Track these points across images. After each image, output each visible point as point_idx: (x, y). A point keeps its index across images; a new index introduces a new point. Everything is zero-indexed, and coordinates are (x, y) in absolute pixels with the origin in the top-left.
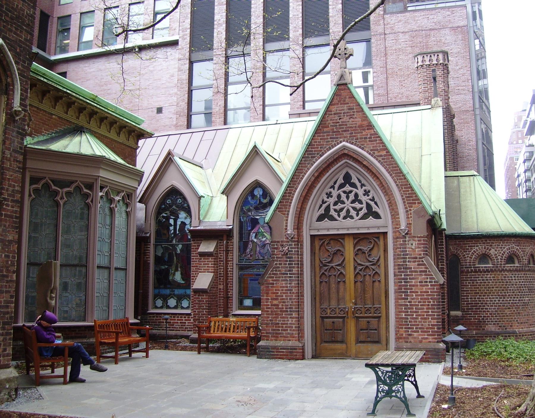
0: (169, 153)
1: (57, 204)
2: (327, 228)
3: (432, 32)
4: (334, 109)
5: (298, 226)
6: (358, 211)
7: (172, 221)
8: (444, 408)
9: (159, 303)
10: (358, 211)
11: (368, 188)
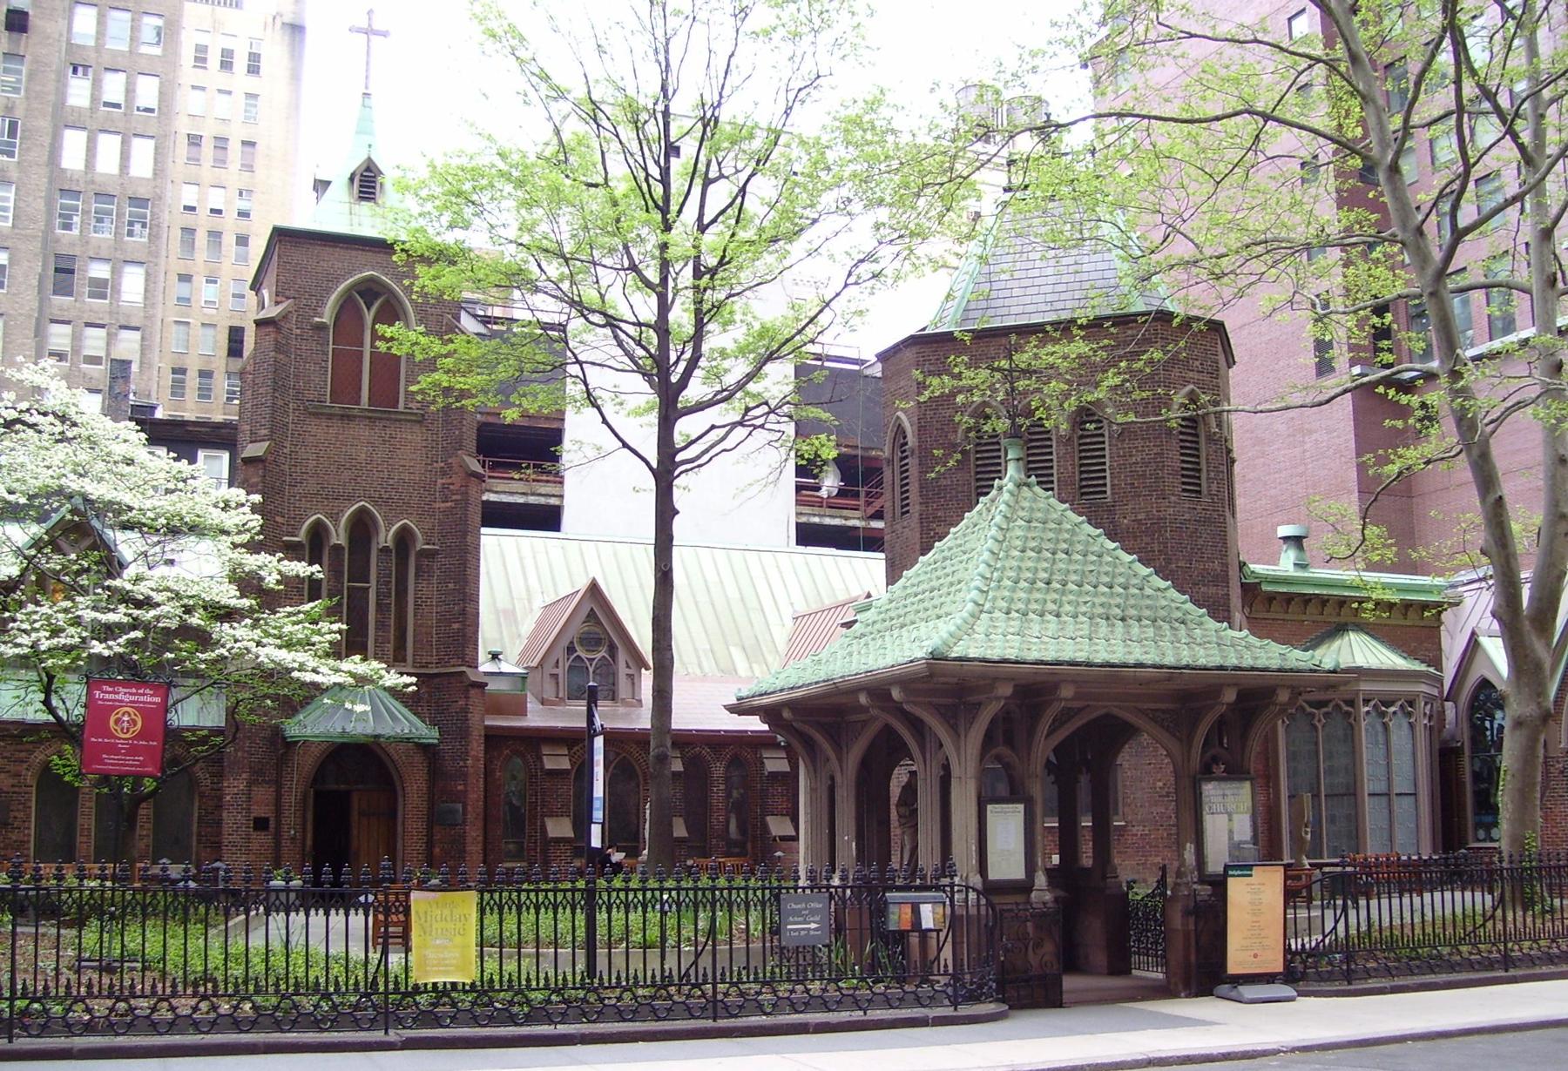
0: (1473, 633)
1: (1316, 728)
7: (1487, 724)
8: (670, 825)
9: (1481, 834)
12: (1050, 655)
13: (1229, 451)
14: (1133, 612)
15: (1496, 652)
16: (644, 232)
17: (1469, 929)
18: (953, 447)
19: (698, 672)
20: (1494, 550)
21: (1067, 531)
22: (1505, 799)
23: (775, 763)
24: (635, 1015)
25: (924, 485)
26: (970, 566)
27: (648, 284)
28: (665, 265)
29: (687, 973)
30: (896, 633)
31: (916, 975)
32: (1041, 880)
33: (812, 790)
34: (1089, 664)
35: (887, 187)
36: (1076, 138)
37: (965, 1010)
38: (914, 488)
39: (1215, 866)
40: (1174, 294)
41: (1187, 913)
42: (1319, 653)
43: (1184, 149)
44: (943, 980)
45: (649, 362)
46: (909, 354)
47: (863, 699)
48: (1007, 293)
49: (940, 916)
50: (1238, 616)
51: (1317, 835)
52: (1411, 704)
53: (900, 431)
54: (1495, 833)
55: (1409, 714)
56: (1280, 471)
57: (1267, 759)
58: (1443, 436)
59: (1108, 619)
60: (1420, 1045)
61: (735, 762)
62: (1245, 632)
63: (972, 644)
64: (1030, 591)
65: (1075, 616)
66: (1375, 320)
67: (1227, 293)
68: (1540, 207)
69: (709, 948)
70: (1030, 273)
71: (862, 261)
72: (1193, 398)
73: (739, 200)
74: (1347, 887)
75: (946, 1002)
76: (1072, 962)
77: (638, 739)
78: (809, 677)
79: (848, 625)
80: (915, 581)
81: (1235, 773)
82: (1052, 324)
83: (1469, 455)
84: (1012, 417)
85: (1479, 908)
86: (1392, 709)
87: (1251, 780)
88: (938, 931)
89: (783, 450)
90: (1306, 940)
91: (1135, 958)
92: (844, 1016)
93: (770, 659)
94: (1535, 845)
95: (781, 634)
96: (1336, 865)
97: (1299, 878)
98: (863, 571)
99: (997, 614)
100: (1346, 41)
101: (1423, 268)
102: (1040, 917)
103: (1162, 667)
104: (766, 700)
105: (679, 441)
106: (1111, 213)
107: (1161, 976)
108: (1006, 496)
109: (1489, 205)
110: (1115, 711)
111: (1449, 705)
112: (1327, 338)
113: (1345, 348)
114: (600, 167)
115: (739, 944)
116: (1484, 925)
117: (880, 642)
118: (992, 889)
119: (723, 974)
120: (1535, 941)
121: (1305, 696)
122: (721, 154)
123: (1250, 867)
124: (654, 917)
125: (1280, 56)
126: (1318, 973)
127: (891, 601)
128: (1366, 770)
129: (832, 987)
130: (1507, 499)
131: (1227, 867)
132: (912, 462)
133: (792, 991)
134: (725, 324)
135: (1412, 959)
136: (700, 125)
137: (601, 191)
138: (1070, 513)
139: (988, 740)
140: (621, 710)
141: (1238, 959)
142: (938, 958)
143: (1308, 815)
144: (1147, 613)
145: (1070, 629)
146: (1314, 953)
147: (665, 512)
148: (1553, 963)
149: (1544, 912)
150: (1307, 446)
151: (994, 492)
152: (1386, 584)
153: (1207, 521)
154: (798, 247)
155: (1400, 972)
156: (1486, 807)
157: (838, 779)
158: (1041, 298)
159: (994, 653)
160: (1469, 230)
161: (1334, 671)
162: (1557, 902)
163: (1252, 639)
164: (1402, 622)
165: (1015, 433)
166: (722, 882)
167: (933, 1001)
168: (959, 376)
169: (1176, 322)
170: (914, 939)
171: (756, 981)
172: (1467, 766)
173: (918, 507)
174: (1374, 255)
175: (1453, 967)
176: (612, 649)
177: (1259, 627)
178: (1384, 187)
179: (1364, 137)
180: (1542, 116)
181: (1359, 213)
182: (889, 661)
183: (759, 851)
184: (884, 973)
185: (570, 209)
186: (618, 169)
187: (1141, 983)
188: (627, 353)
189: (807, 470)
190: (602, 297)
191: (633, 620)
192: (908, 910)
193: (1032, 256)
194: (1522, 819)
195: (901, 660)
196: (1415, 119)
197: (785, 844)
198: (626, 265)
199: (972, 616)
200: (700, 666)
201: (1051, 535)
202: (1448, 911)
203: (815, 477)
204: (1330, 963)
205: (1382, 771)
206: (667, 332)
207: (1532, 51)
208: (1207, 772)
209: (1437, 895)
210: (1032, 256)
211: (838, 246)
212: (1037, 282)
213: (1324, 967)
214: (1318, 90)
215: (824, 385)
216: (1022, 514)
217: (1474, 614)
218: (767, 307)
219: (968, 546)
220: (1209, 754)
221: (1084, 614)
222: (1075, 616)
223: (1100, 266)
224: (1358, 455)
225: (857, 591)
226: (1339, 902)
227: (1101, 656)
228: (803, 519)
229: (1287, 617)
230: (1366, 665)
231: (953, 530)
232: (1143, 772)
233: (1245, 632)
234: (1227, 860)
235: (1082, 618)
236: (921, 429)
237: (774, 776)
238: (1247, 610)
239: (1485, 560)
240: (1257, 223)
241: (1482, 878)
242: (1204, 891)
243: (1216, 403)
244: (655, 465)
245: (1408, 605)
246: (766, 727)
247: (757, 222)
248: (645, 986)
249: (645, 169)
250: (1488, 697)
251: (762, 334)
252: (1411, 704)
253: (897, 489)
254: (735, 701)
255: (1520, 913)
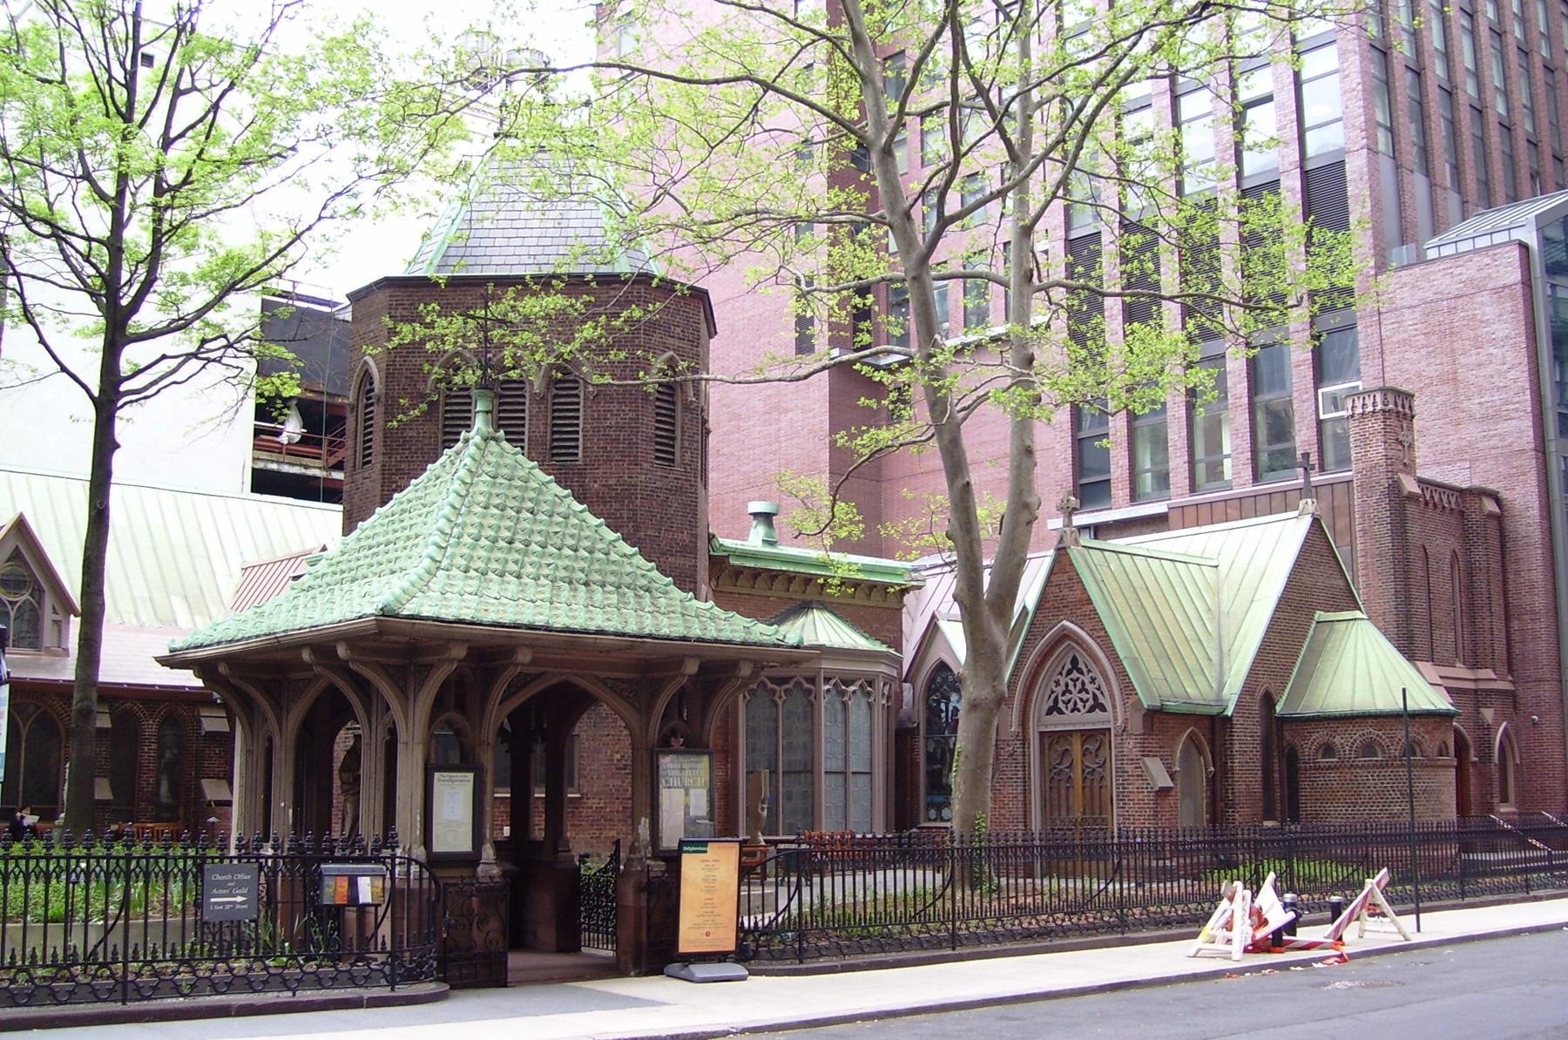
0: (933, 617)
1: (776, 705)
2: (1057, 723)
3: (1460, 301)
4: (1054, 578)
5: (1024, 723)
6: (1084, 702)
7: (943, 706)
10: (1084, 702)
11: (1053, 685)
12: (507, 618)
13: (705, 422)
14: (597, 577)
15: (955, 639)
16: (102, 138)
17: (920, 908)
18: (422, 397)
19: (134, 621)
20: (959, 535)
21: (533, 490)
22: (957, 778)
23: (213, 722)
24: (31, 999)
25: (388, 434)
26: (430, 519)
27: (103, 197)
28: (122, 179)
29: (94, 952)
30: (346, 587)
31: (351, 953)
32: (488, 853)
33: (248, 752)
34: (548, 629)
35: (372, 113)
36: (575, 86)
37: (403, 990)
38: (378, 437)
39: (669, 841)
40: (656, 257)
41: (639, 889)
42: (783, 629)
43: (679, 109)
44: (381, 958)
45: (98, 282)
46: (382, 297)
47: (306, 655)
48: (489, 242)
49: (379, 890)
50: (704, 589)
51: (773, 812)
52: (870, 684)
53: (367, 376)
54: (945, 813)
55: (869, 694)
56: (753, 448)
57: (727, 734)
58: (917, 420)
59: (570, 583)
60: (868, 1024)
61: (170, 720)
62: (711, 603)
63: (425, 601)
64: (491, 550)
65: (536, 579)
66: (857, 300)
67: (714, 259)
68: (1022, 204)
69: (121, 922)
70: (516, 224)
71: (338, 194)
72: (672, 364)
73: (211, 116)
74: (802, 864)
75: (383, 981)
76: (519, 940)
77: (61, 691)
78: (250, 630)
79: (296, 578)
80: (368, 533)
81: (694, 746)
82: (533, 277)
83: (940, 440)
84: (484, 368)
85: (929, 886)
86: (852, 688)
87: (710, 754)
88: (377, 906)
89: (241, 388)
90: (759, 917)
91: (585, 936)
92: (271, 997)
93: (214, 611)
94: (985, 826)
95: (229, 584)
96: (792, 842)
97: (754, 854)
98: (319, 522)
99: (455, 572)
100: (851, 21)
101: (908, 252)
102: (488, 893)
103: (624, 635)
104: (201, 653)
105: (125, 368)
106: (602, 169)
107: (611, 953)
108: (472, 449)
109: (971, 200)
110: (573, 679)
111: (907, 686)
112: (809, 314)
113: (826, 326)
114: (58, 65)
115: (156, 917)
116: (933, 903)
117: (328, 596)
118: (436, 862)
119: (135, 952)
120: (982, 920)
121: (767, 672)
122: (196, 64)
123: (705, 843)
124: (58, 885)
125: (784, 27)
126: (769, 951)
127: (343, 553)
128: (824, 748)
129: (257, 965)
130: (974, 488)
131: (682, 843)
132: (378, 410)
133: (213, 970)
134: (188, 248)
135: (863, 938)
136: (174, 32)
137: (55, 90)
138: (537, 472)
139: (439, 704)
140: (45, 659)
141: (690, 937)
142: (375, 935)
143: (765, 791)
144: (612, 579)
145: (531, 592)
146: (767, 931)
147: (105, 445)
148: (998, 942)
149: (991, 891)
150: (782, 424)
151: (460, 445)
152: (850, 564)
153: (680, 490)
154: (269, 176)
155: (850, 950)
156: (939, 787)
157: (277, 739)
158: (524, 251)
159: (449, 613)
160: (953, 219)
161: (797, 647)
162: (1003, 881)
163: (717, 611)
164: (866, 603)
165: (485, 385)
166: (138, 850)
167: (368, 980)
168: (431, 325)
169: (655, 283)
170: (351, 914)
171: (173, 959)
172: (922, 747)
173: (380, 458)
174: (860, 236)
175: (902, 946)
176: (38, 592)
177: (724, 599)
178: (875, 171)
179: (860, 120)
180: (1030, 117)
181: (851, 193)
182: (336, 616)
183: (193, 820)
184: (322, 948)
185: (17, 104)
186: (77, 66)
187: (591, 961)
188: (74, 270)
189: (267, 411)
190: (50, 205)
191: (65, 561)
192: (344, 883)
193: (518, 206)
194: (973, 801)
195: (349, 616)
196: (911, 107)
197: (220, 810)
198: (80, 172)
199: (428, 572)
200: (136, 615)
201: (517, 493)
202: (900, 890)
203: (274, 420)
204: (782, 942)
205: (839, 750)
206: (120, 250)
207: (1025, 52)
208: (665, 745)
209: (890, 873)
210: (518, 206)
211: (315, 175)
212: (521, 233)
213: (776, 946)
214: (821, 69)
215: (289, 323)
216: (487, 469)
217: (936, 600)
218: (233, 231)
219: (428, 499)
220: (670, 725)
221: (546, 577)
222: (536, 579)
223: (588, 223)
224: (833, 430)
225: (313, 544)
226: (794, 879)
227: (561, 620)
228: (260, 465)
229: (754, 592)
230: (828, 644)
231: (413, 481)
232: (600, 743)
233: (711, 603)
234: (682, 836)
235: (543, 581)
236: (389, 376)
237: (212, 736)
238: (713, 583)
239: (950, 543)
240: (749, 192)
241: (933, 858)
242: (658, 867)
243: (695, 371)
244: (96, 394)
245: (873, 586)
246: (199, 683)
247: (229, 141)
248: (45, 966)
249: (108, 70)
250: (945, 680)
251: (227, 261)
252: (870, 684)
253: (360, 439)
254: (166, 653)
255: (968, 892)
